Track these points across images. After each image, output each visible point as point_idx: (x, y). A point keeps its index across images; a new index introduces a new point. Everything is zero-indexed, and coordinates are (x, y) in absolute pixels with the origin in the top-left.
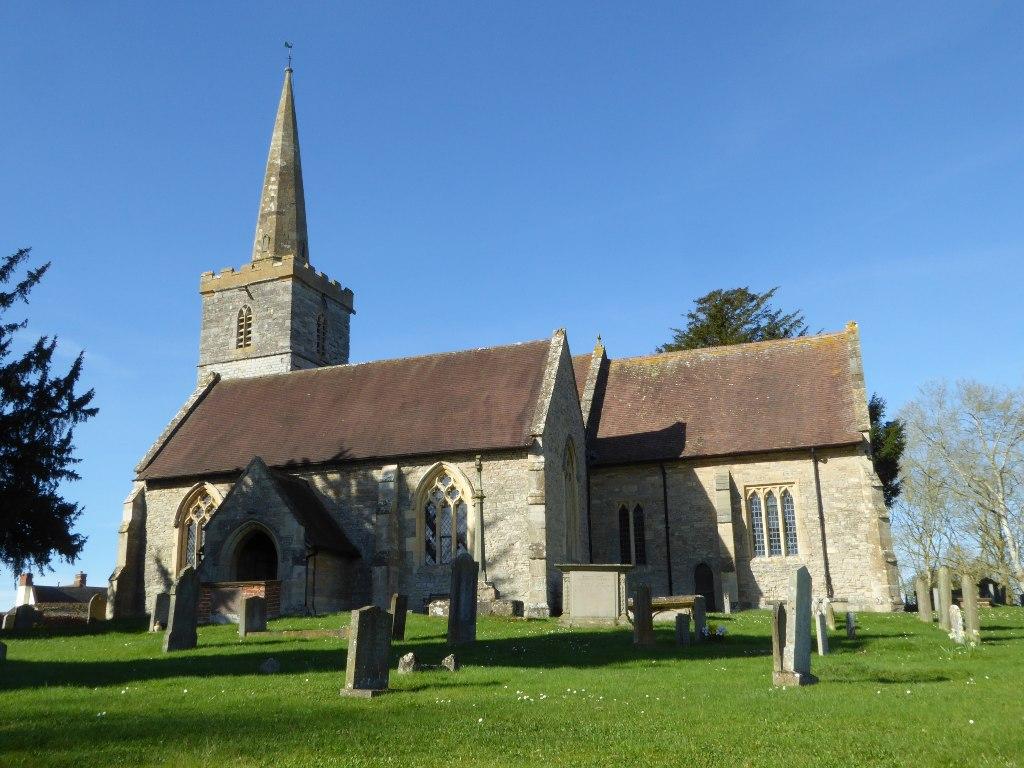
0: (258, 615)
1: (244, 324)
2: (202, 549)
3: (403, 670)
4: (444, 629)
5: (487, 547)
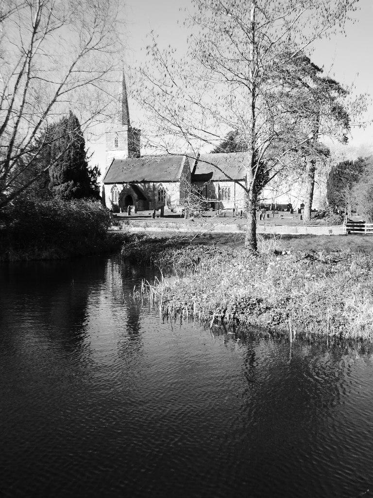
0: (136, 210)
1: (116, 141)
5: (197, 170)
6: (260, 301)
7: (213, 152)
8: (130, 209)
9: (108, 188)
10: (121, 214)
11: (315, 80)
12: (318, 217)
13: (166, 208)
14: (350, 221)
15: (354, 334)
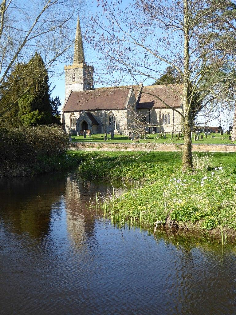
0: (91, 134)
2: (76, 124)
3: (107, 140)
4: (111, 136)
5: (141, 98)
6: (195, 210)
8: (86, 133)
9: (67, 115)
10: (78, 137)
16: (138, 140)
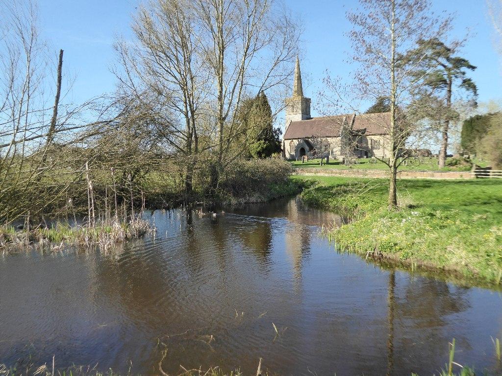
0: (308, 159)
6: (396, 244)
7: (367, 113)
8: (304, 158)
9: (287, 143)
10: (296, 162)
11: (448, 59)
12: (451, 164)
13: (330, 157)
14: (479, 168)
15: (452, 268)
16: (351, 165)
